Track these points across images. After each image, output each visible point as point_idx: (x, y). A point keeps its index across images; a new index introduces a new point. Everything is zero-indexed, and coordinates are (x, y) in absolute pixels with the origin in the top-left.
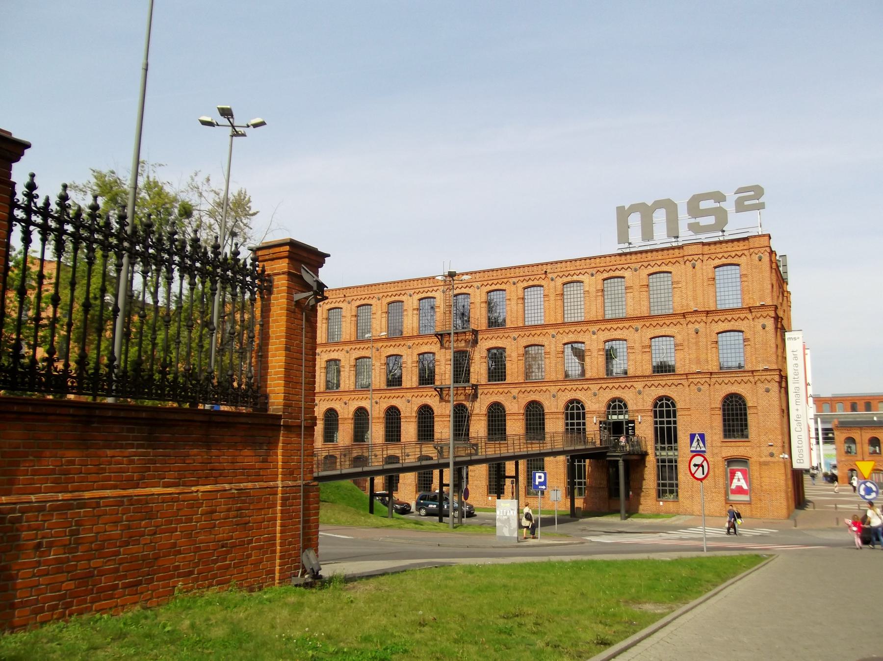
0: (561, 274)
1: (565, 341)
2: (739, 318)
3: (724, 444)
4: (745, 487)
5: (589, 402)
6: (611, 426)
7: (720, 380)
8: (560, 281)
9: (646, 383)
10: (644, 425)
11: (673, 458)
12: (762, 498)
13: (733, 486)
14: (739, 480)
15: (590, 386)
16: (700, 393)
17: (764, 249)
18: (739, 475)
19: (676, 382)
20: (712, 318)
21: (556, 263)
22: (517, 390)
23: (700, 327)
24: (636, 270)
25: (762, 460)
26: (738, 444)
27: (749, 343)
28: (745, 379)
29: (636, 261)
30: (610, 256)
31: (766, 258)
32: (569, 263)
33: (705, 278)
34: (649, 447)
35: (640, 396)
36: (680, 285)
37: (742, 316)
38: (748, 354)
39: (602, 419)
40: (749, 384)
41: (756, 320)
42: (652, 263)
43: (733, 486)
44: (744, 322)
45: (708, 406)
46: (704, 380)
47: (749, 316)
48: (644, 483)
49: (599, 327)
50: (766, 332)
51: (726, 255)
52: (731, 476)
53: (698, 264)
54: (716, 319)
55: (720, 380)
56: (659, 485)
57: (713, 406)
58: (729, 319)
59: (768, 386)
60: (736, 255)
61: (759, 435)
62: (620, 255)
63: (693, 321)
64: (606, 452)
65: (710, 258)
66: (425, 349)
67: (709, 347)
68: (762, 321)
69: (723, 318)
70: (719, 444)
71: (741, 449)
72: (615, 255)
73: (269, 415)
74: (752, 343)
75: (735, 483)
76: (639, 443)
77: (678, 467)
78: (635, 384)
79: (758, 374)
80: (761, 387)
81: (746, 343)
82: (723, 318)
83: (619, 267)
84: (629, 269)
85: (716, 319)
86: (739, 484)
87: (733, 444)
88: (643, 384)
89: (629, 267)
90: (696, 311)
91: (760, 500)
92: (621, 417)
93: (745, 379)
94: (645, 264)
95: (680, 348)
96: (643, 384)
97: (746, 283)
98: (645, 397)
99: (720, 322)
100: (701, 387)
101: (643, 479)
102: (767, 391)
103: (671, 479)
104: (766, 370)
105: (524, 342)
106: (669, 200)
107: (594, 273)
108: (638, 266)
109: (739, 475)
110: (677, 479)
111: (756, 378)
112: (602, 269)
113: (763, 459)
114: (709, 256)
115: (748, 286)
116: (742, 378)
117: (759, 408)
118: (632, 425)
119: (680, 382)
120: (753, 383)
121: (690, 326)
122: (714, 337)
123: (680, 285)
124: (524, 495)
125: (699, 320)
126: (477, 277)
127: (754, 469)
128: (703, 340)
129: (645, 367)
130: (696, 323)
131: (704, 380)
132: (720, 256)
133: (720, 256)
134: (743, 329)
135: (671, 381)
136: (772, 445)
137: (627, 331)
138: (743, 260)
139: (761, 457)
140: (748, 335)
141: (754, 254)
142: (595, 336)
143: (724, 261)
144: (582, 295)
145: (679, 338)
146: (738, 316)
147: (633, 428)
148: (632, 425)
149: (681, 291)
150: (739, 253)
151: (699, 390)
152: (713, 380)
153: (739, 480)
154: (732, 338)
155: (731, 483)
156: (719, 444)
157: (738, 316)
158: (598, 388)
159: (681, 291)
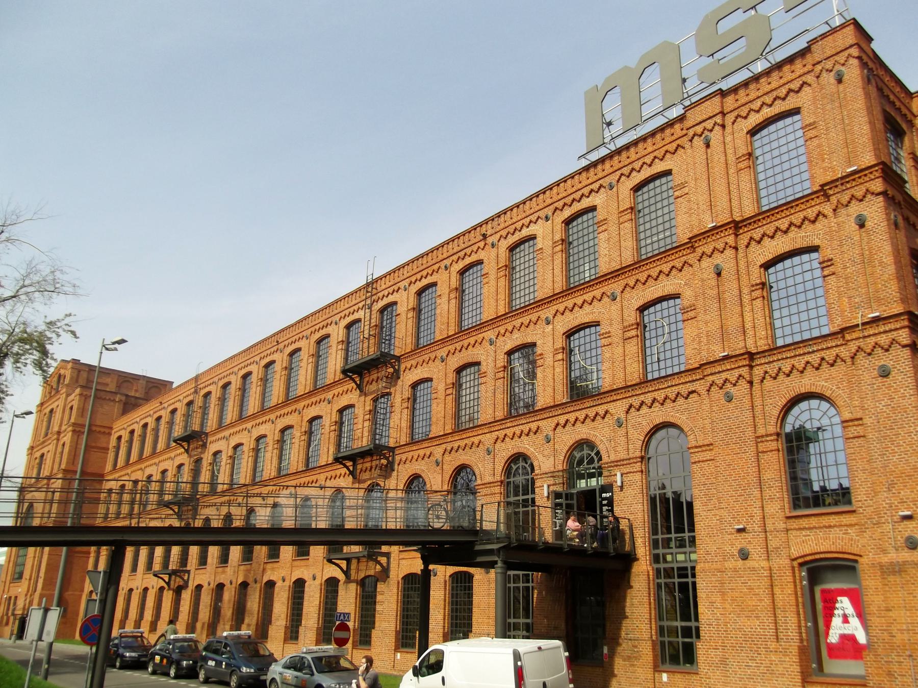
0: (504, 233)
1: (508, 347)
2: (805, 219)
3: (794, 524)
4: (862, 638)
5: (540, 457)
6: (575, 502)
7: (772, 369)
8: (504, 245)
9: (630, 401)
10: (628, 491)
11: (689, 565)
12: (895, 668)
13: (833, 638)
14: (846, 620)
15: (540, 423)
16: (731, 405)
17: (846, 53)
18: (844, 604)
19: (684, 390)
20: (749, 235)
21: (499, 215)
22: (440, 450)
23: (725, 260)
24: (611, 187)
25: (885, 559)
26: (825, 520)
27: (832, 269)
28: (829, 355)
29: (611, 170)
30: (572, 177)
31: (853, 72)
32: (515, 210)
33: (731, 158)
34: (639, 542)
35: (622, 431)
36: (686, 190)
37: (811, 213)
38: (833, 295)
39: (559, 489)
40: (840, 367)
41: (842, 211)
42: (637, 165)
43: (833, 638)
44: (818, 225)
45: (749, 432)
46: (736, 373)
47: (827, 209)
48: (626, 624)
49: (555, 308)
50: (867, 233)
51: (768, 100)
52: (825, 608)
53: (716, 136)
54: (757, 235)
55: (772, 369)
56: (661, 630)
57: (761, 431)
58: (784, 227)
59: (885, 360)
60: (790, 91)
61: (876, 493)
62: (586, 169)
63: (709, 252)
64: (472, 543)
65: (738, 116)
66: (344, 401)
67: (746, 299)
68: (855, 209)
69: (769, 230)
70: (782, 526)
71: (836, 533)
72: (579, 173)
73: (235, 528)
74: (837, 268)
75: (837, 630)
76: (617, 533)
77: (699, 586)
78: (611, 407)
79: (854, 335)
80: (867, 367)
81: (826, 272)
82: (769, 230)
83: (586, 191)
84: (602, 190)
85: (757, 235)
86: (848, 630)
87: (814, 521)
88: (624, 405)
89: (601, 186)
90: (715, 228)
91: (890, 674)
92: (593, 482)
93: (829, 355)
94: (626, 171)
95: (692, 314)
96: (624, 405)
97: (816, 142)
98: (631, 431)
99: (766, 240)
100: (733, 391)
101: (623, 616)
102: (885, 373)
103: (469, 583)
104: (876, 320)
105: (455, 362)
106: (665, 42)
107: (550, 214)
108: (614, 178)
109: (844, 604)
110: (697, 619)
111: (853, 347)
112: (561, 203)
113: (893, 556)
114: (735, 113)
115: (819, 146)
116: (822, 354)
117: (867, 421)
118: (608, 495)
119: (691, 387)
120: (849, 360)
121: (706, 262)
122: (756, 275)
123: (686, 190)
124: (282, 635)
125: (720, 246)
126: (405, 272)
127: (870, 582)
128: (730, 286)
129: (628, 369)
130: (716, 254)
131: (736, 373)
132: (756, 105)
133: (756, 105)
134: (817, 242)
135: (675, 390)
136: (909, 518)
137: (601, 304)
138: (803, 99)
139: (884, 551)
140: (827, 253)
141: (824, 74)
142: (550, 327)
143: (767, 112)
144: (680, 317)
145: (688, 295)
146: (801, 215)
147: (610, 502)
148: (608, 495)
149: (689, 201)
150: (795, 86)
151: (729, 399)
152: (758, 372)
153: (846, 620)
154: (798, 270)
155: (828, 625)
156: (782, 526)
157: (801, 215)
158: (553, 425)
159: (689, 201)
